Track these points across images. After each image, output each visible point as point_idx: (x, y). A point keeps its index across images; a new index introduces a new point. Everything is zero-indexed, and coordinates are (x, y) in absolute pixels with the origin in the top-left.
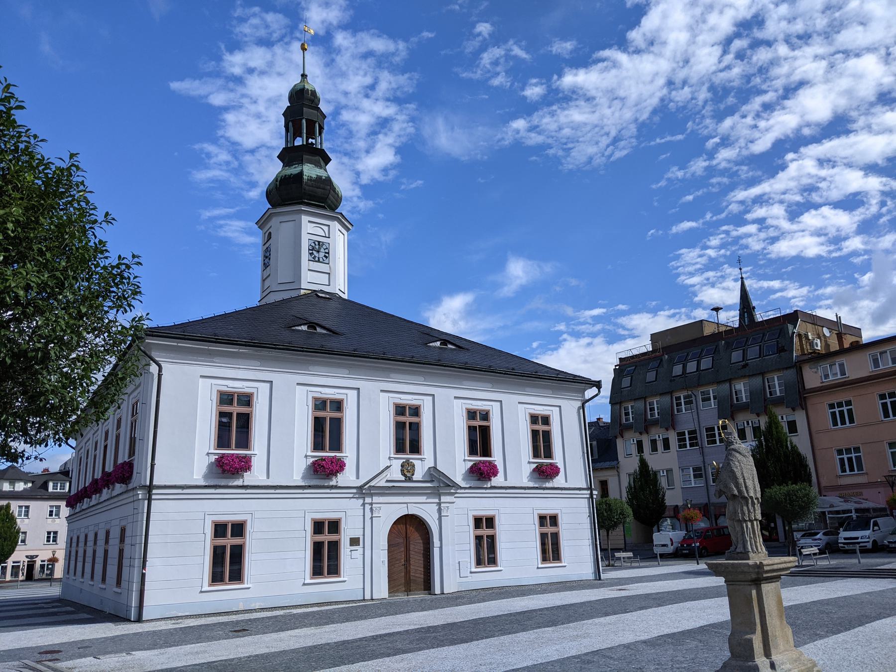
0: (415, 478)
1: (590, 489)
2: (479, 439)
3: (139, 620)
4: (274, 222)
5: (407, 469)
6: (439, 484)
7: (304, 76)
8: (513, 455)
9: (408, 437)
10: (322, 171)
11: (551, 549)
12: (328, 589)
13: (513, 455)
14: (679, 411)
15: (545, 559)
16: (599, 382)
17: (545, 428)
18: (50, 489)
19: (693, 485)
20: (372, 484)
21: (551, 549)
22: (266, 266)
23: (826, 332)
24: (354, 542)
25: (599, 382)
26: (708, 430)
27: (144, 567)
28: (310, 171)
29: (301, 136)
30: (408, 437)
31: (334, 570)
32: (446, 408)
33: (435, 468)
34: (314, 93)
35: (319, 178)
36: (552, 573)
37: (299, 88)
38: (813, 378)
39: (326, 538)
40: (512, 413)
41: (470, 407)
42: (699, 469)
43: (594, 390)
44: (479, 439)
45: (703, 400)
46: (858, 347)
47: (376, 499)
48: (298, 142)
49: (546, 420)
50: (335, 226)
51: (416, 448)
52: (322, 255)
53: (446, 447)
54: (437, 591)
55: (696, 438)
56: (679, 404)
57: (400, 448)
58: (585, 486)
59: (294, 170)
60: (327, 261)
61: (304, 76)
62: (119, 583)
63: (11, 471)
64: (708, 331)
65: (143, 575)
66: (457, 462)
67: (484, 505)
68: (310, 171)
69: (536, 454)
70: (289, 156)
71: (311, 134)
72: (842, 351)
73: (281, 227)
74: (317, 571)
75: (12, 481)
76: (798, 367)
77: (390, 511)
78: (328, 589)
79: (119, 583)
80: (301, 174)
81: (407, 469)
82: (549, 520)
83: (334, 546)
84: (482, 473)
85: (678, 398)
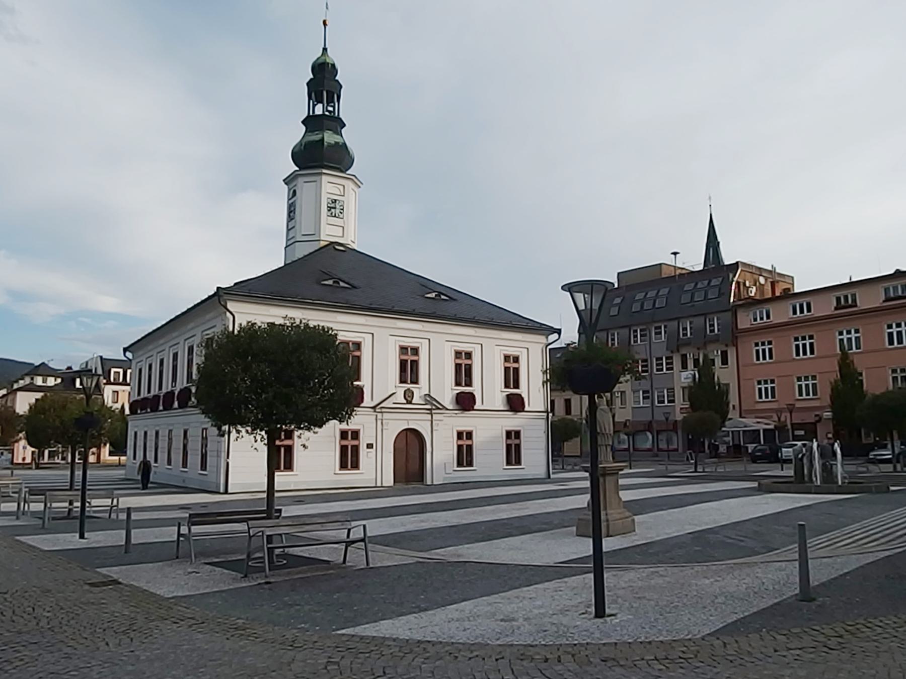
0: (414, 402)
1: (547, 412)
2: (463, 374)
3: (226, 492)
4: (301, 180)
5: (409, 396)
6: (433, 405)
7: (325, 49)
8: (490, 388)
9: (409, 370)
10: (339, 137)
11: (513, 454)
12: (350, 478)
13: (490, 388)
14: (636, 342)
15: (509, 463)
16: (560, 330)
17: (516, 365)
18: (78, 385)
19: (642, 405)
20: (382, 405)
21: (513, 454)
22: (290, 218)
23: (762, 280)
24: (370, 446)
25: (560, 330)
26: (657, 359)
27: (228, 457)
28: (329, 138)
29: (322, 102)
30: (409, 370)
31: (356, 466)
32: (439, 344)
33: (429, 395)
34: (333, 65)
35: (337, 143)
36: (514, 472)
37: (320, 61)
38: (745, 320)
39: (350, 443)
40: (490, 350)
41: (506, 353)
42: (647, 392)
43: (556, 336)
44: (463, 374)
45: (656, 333)
46: (788, 294)
47: (386, 416)
48: (319, 110)
49: (516, 359)
50: (349, 185)
51: (415, 381)
52: (338, 211)
53: (438, 380)
54: (429, 483)
55: (647, 366)
56: (636, 336)
57: (403, 381)
58: (543, 409)
59: (316, 137)
60: (341, 216)
61: (325, 49)
62: (204, 466)
63: (41, 367)
64: (666, 273)
65: (228, 464)
66: (447, 393)
67: (465, 421)
68: (329, 138)
69: (507, 386)
70: (311, 122)
71: (330, 101)
72: (774, 299)
73: (305, 188)
74: (343, 466)
75: (45, 376)
76: (734, 310)
77: (395, 425)
78: (350, 478)
79: (204, 466)
80: (323, 139)
81: (409, 396)
82: (513, 435)
83: (356, 449)
84: (465, 402)
85: (636, 331)
